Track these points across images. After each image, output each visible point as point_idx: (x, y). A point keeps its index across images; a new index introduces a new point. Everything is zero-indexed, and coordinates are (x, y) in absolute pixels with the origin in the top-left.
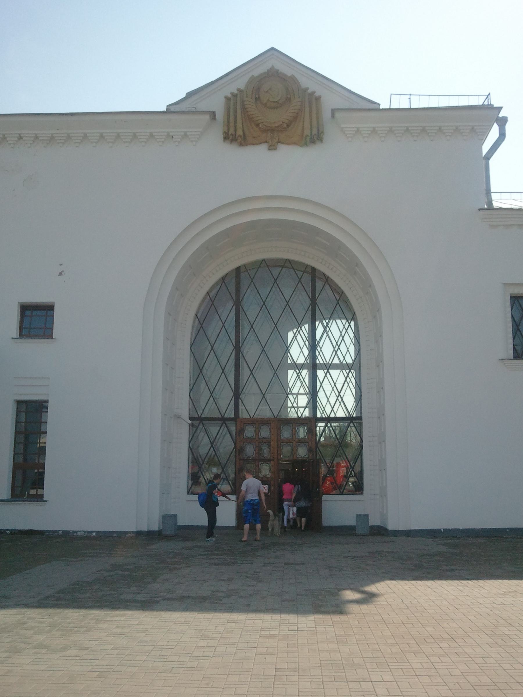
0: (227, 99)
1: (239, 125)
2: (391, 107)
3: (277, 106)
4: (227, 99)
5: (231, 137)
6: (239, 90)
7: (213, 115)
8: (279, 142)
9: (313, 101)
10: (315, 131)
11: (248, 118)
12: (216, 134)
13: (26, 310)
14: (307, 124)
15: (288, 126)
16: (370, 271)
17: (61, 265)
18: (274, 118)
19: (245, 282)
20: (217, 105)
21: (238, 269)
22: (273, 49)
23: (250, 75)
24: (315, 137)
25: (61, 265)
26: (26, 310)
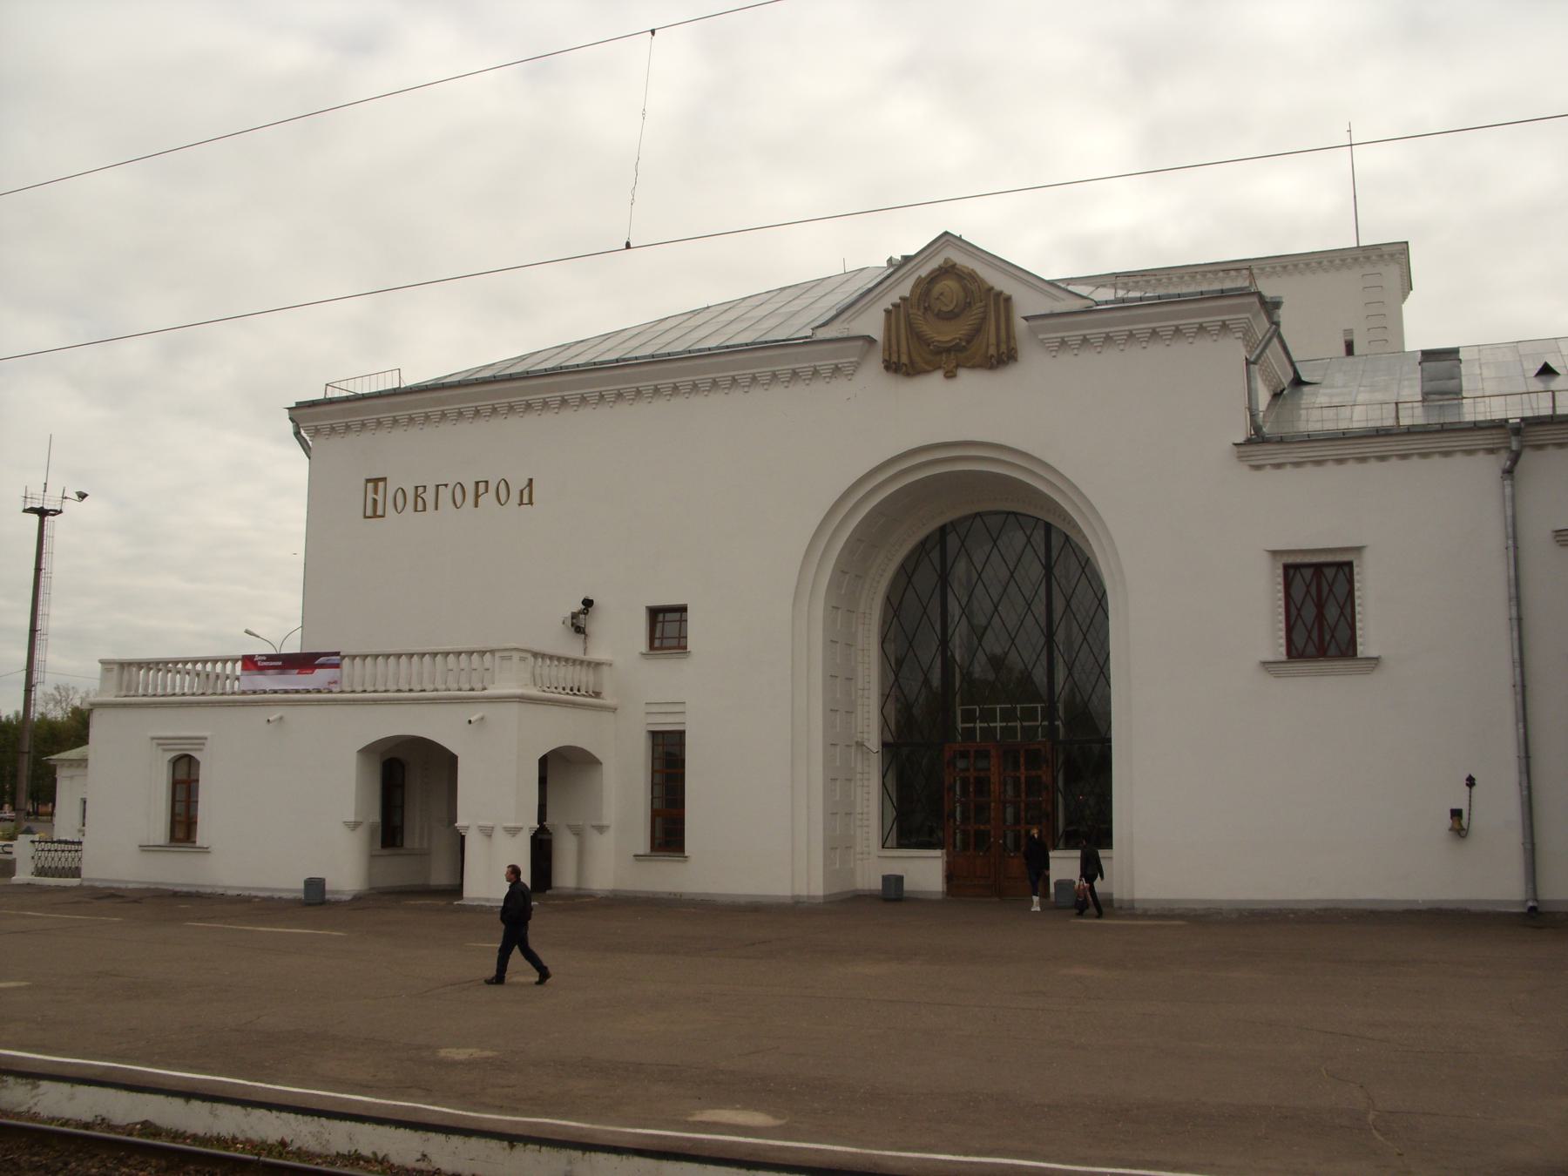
0: (887, 312)
1: (904, 349)
2: (1559, 411)
3: (951, 316)
4: (887, 312)
5: (893, 366)
6: (903, 299)
7: (870, 340)
8: (957, 366)
9: (1003, 302)
10: (1003, 348)
11: (916, 336)
12: (875, 363)
13: (655, 613)
14: (993, 340)
15: (968, 342)
16: (1086, 531)
17: (1350, 349)
18: (946, 334)
19: (953, 542)
20: (872, 324)
21: (943, 530)
22: (946, 233)
23: (916, 276)
24: (1003, 357)
25: (1350, 349)
26: (655, 613)
